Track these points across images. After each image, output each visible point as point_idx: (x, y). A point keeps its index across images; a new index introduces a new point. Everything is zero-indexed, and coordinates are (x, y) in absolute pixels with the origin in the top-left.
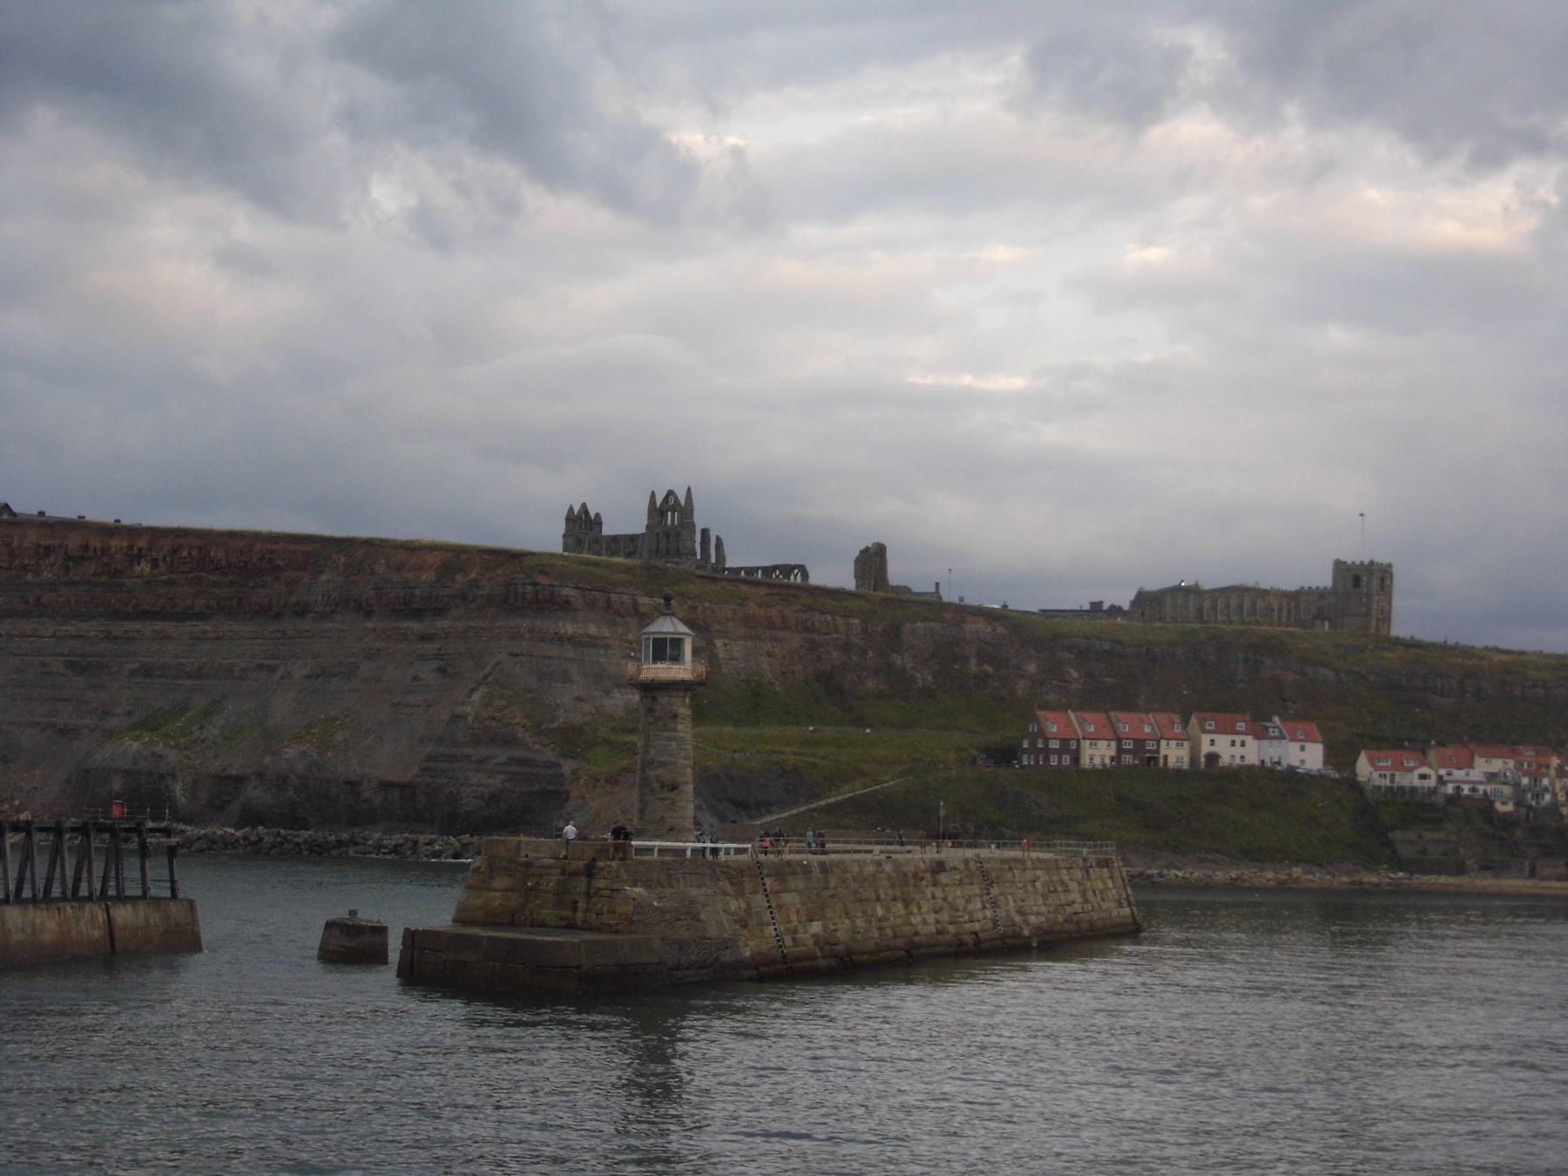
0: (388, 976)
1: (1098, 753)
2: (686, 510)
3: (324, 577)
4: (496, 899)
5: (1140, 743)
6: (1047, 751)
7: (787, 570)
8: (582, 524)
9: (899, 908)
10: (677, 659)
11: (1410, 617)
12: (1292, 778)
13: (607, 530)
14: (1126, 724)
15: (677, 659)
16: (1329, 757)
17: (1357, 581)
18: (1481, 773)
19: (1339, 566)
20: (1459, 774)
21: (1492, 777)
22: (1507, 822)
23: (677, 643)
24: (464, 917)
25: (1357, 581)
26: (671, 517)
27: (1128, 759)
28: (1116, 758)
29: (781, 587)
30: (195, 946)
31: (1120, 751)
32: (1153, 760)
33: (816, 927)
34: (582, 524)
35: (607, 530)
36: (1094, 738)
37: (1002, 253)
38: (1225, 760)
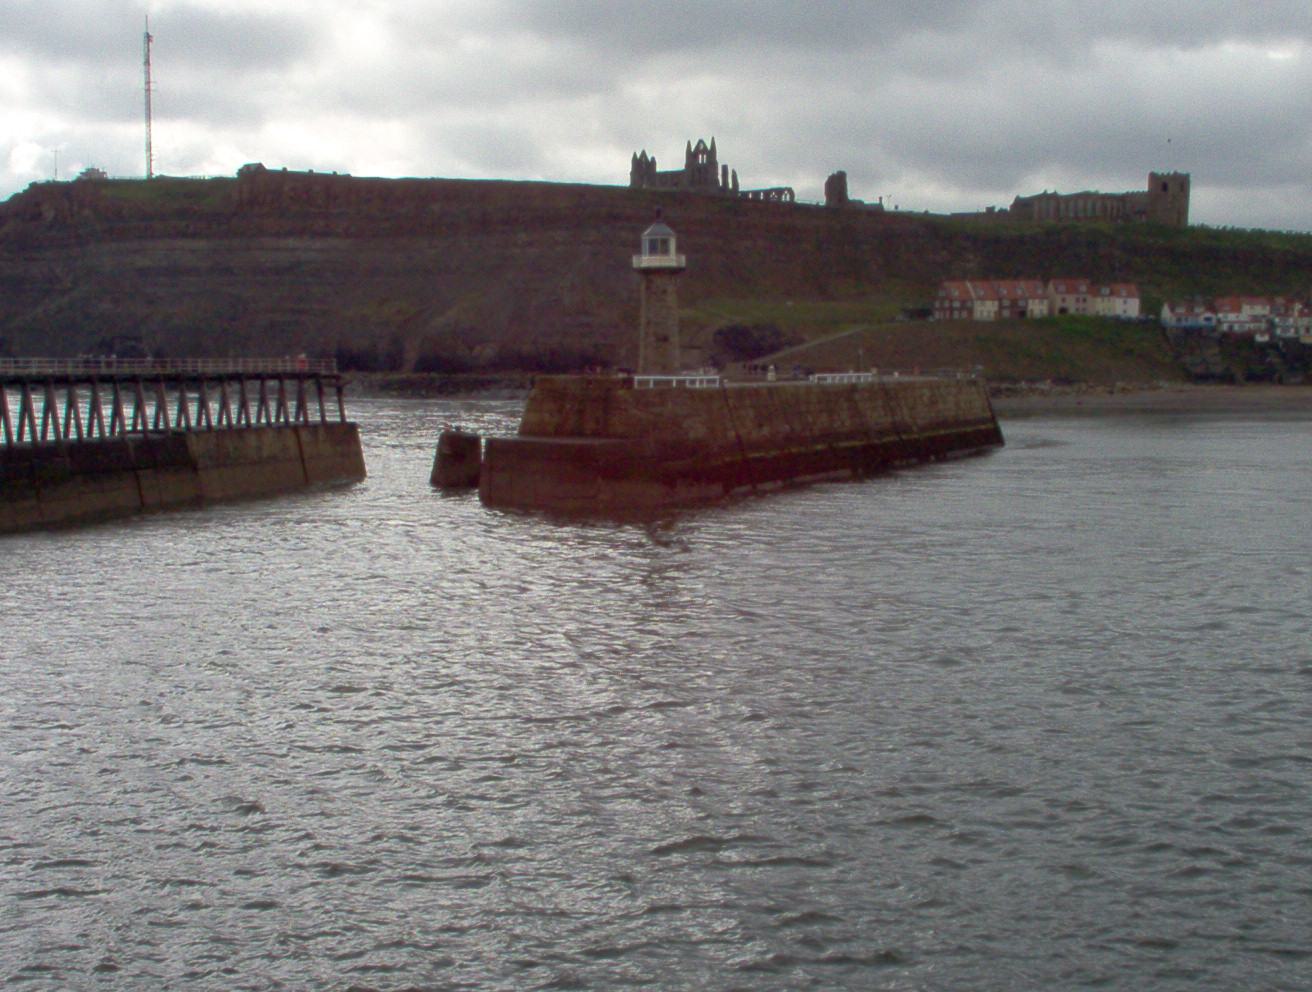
5: (1014, 303)
6: (951, 309)
7: (780, 191)
8: (642, 166)
10: (666, 251)
12: (1121, 323)
13: (660, 168)
15: (666, 251)
18: (1244, 316)
19: (1153, 177)
20: (1232, 317)
21: (1255, 319)
22: (1263, 349)
23: (665, 242)
24: (525, 430)
25: (1165, 187)
27: (1006, 313)
28: (999, 313)
30: (357, 472)
31: (1001, 307)
32: (1023, 313)
34: (642, 166)
35: (660, 168)
36: (982, 299)
38: (1072, 311)
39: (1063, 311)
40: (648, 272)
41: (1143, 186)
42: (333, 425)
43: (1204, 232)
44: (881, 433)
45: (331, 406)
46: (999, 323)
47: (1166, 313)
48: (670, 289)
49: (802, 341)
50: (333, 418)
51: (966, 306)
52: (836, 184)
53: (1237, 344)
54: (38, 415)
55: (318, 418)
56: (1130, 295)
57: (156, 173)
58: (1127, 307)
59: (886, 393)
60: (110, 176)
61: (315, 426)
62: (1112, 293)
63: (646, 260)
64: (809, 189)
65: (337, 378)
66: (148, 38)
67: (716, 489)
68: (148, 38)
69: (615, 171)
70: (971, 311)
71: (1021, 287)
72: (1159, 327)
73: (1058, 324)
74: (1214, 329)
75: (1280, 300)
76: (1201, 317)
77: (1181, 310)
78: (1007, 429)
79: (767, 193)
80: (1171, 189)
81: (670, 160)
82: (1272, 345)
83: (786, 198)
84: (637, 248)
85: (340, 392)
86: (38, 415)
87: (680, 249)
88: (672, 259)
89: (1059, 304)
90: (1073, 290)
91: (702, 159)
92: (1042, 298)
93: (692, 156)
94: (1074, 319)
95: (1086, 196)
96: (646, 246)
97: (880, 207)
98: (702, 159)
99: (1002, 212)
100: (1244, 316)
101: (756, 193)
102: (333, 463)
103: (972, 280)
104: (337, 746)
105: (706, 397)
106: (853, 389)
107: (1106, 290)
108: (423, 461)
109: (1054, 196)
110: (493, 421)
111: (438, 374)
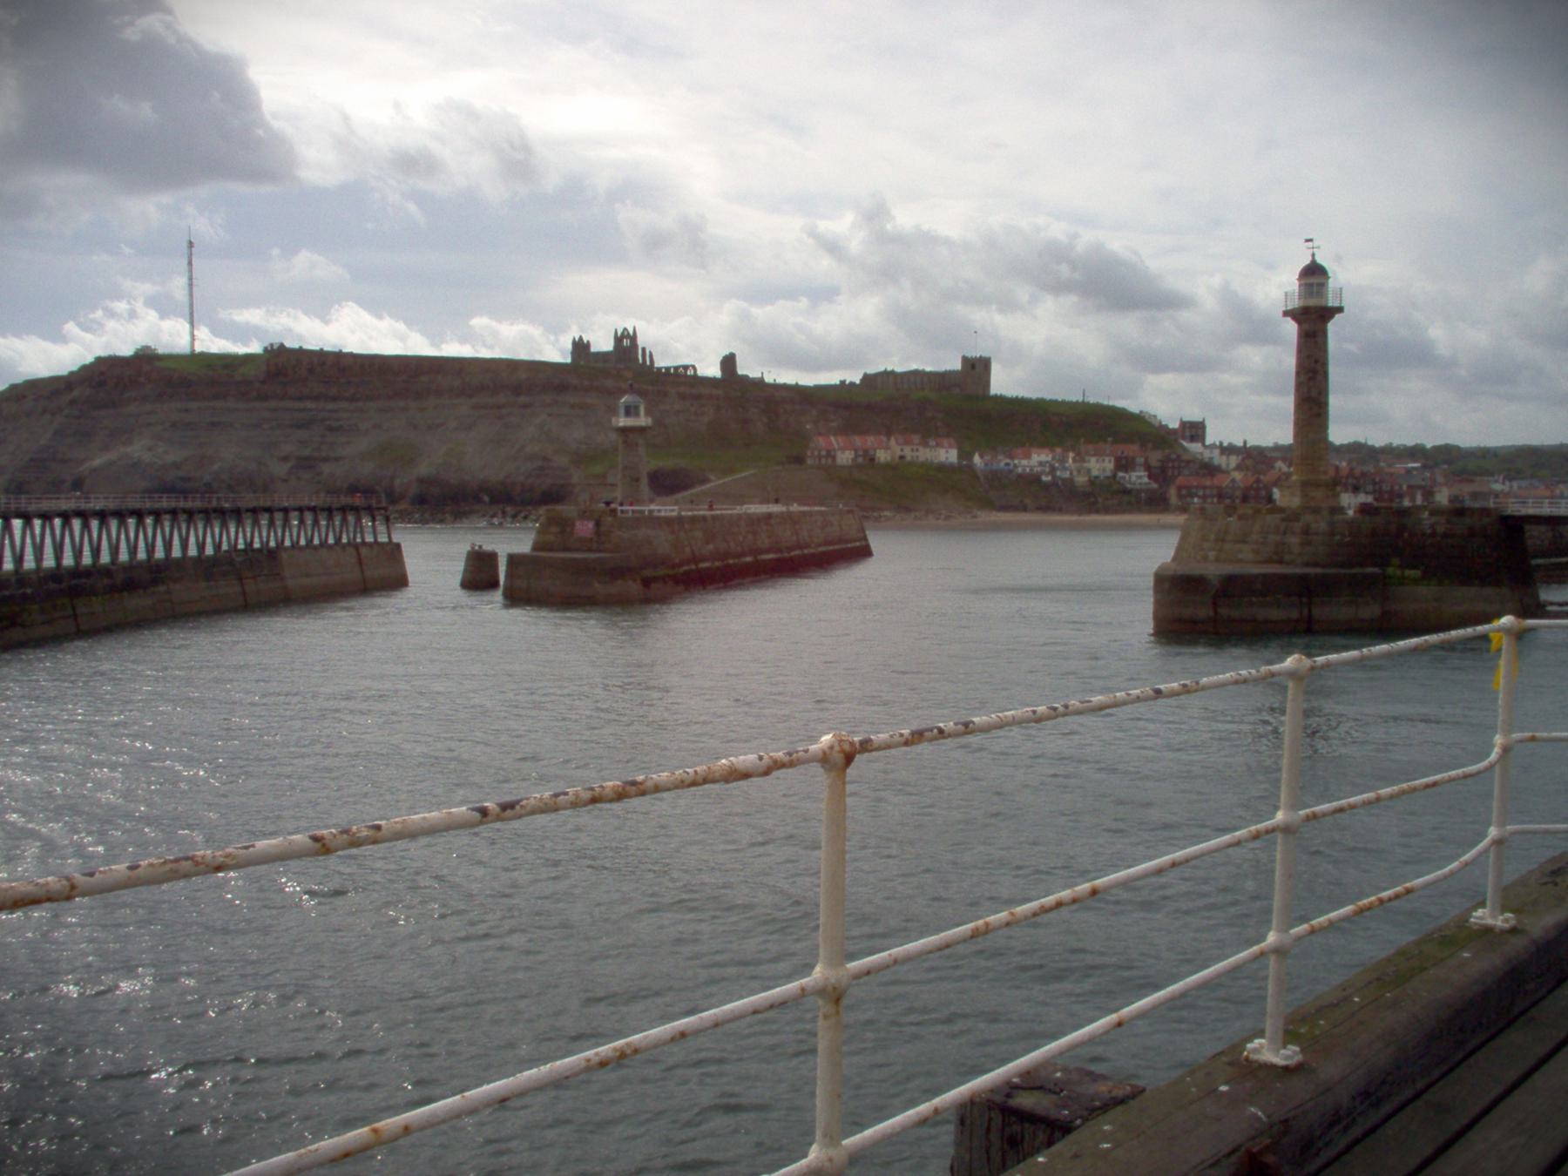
0: (498, 596)
1: (845, 458)
2: (634, 338)
3: (55, 826)
4: (552, 538)
5: (866, 452)
6: (820, 457)
7: (686, 367)
8: (580, 347)
9: (750, 536)
10: (637, 415)
11: (1002, 383)
12: (942, 468)
13: (593, 349)
14: (858, 441)
15: (637, 415)
16: (960, 456)
17: (973, 367)
18: (1036, 460)
19: (965, 360)
20: (1024, 462)
21: (1041, 464)
22: (1047, 487)
23: (637, 408)
24: (536, 548)
25: (973, 367)
26: (626, 344)
27: (860, 460)
28: (854, 460)
29: (681, 381)
30: (398, 582)
31: (857, 456)
32: (872, 459)
33: (711, 547)
34: (580, 347)
35: (593, 349)
36: (843, 449)
37: (1040, 1159)
38: (909, 458)
39: (902, 457)
40: (624, 431)
41: (955, 365)
42: (382, 544)
43: (1001, 400)
44: (790, 549)
45: (381, 528)
46: (855, 466)
47: (977, 459)
48: (641, 441)
49: (705, 481)
50: (383, 539)
51: (830, 454)
52: (729, 362)
53: (1031, 479)
54: (141, 544)
55: (385, 540)
56: (950, 446)
57: (198, 349)
58: (948, 455)
59: (789, 518)
60: (160, 351)
61: (370, 545)
62: (938, 445)
63: (623, 421)
64: (711, 370)
65: (385, 509)
66: (191, 244)
67: (633, 587)
68: (191, 244)
69: (556, 352)
70: (834, 458)
71: (871, 440)
72: (971, 468)
73: (897, 469)
74: (1011, 471)
75: (1059, 450)
76: (1002, 462)
77: (987, 458)
78: (876, 541)
79: (676, 368)
80: (978, 368)
81: (602, 343)
82: (1054, 484)
83: (690, 372)
84: (613, 411)
85: (387, 520)
86: (141, 544)
87: (648, 413)
88: (643, 420)
89: (899, 453)
90: (907, 443)
91: (626, 342)
92: (887, 448)
93: (618, 340)
94: (911, 464)
95: (916, 373)
96: (622, 411)
97: (762, 380)
98: (626, 342)
99: (852, 384)
100: (1036, 460)
101: (668, 369)
102: (387, 577)
103: (835, 435)
104: (931, 740)
105: (669, 522)
106: (769, 516)
107: (932, 443)
108: (457, 568)
109: (893, 372)
110: (511, 542)
111: (443, 502)
